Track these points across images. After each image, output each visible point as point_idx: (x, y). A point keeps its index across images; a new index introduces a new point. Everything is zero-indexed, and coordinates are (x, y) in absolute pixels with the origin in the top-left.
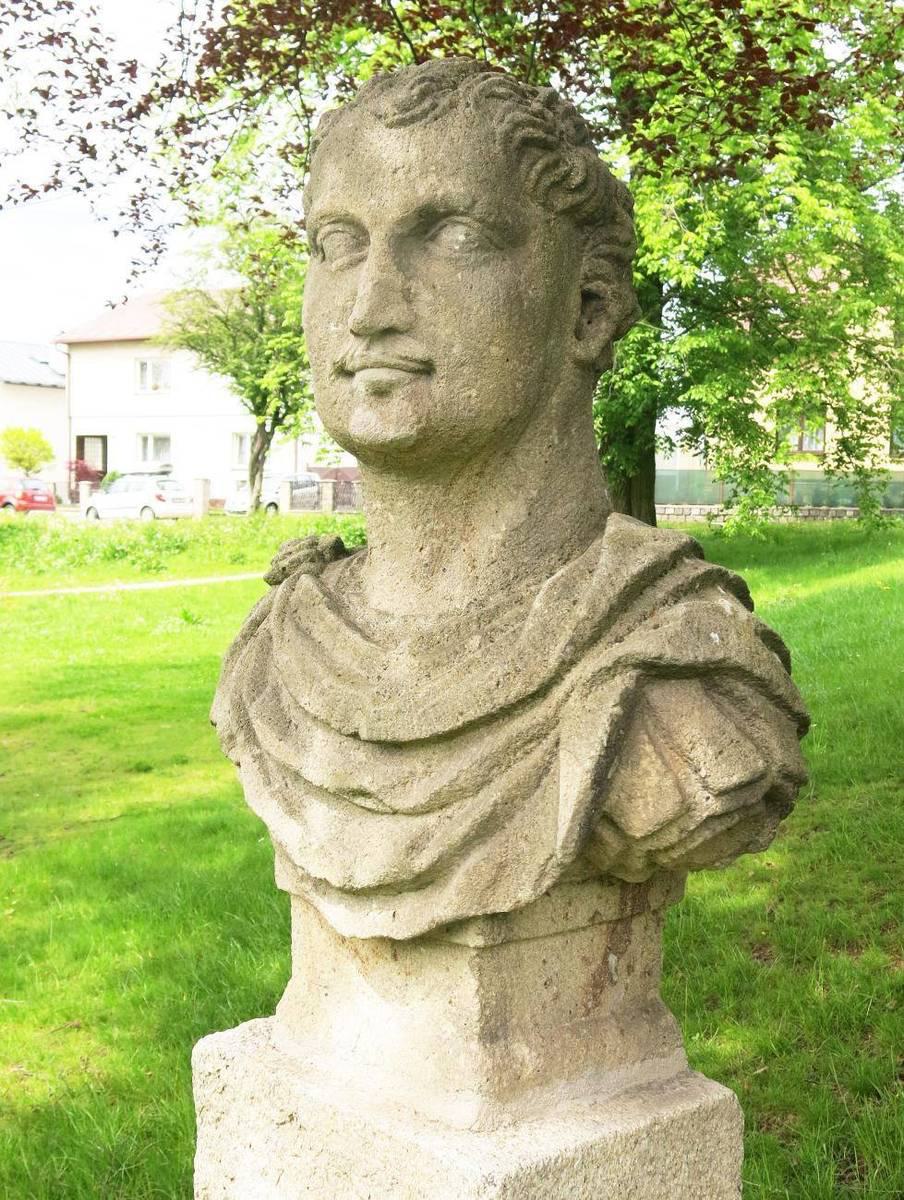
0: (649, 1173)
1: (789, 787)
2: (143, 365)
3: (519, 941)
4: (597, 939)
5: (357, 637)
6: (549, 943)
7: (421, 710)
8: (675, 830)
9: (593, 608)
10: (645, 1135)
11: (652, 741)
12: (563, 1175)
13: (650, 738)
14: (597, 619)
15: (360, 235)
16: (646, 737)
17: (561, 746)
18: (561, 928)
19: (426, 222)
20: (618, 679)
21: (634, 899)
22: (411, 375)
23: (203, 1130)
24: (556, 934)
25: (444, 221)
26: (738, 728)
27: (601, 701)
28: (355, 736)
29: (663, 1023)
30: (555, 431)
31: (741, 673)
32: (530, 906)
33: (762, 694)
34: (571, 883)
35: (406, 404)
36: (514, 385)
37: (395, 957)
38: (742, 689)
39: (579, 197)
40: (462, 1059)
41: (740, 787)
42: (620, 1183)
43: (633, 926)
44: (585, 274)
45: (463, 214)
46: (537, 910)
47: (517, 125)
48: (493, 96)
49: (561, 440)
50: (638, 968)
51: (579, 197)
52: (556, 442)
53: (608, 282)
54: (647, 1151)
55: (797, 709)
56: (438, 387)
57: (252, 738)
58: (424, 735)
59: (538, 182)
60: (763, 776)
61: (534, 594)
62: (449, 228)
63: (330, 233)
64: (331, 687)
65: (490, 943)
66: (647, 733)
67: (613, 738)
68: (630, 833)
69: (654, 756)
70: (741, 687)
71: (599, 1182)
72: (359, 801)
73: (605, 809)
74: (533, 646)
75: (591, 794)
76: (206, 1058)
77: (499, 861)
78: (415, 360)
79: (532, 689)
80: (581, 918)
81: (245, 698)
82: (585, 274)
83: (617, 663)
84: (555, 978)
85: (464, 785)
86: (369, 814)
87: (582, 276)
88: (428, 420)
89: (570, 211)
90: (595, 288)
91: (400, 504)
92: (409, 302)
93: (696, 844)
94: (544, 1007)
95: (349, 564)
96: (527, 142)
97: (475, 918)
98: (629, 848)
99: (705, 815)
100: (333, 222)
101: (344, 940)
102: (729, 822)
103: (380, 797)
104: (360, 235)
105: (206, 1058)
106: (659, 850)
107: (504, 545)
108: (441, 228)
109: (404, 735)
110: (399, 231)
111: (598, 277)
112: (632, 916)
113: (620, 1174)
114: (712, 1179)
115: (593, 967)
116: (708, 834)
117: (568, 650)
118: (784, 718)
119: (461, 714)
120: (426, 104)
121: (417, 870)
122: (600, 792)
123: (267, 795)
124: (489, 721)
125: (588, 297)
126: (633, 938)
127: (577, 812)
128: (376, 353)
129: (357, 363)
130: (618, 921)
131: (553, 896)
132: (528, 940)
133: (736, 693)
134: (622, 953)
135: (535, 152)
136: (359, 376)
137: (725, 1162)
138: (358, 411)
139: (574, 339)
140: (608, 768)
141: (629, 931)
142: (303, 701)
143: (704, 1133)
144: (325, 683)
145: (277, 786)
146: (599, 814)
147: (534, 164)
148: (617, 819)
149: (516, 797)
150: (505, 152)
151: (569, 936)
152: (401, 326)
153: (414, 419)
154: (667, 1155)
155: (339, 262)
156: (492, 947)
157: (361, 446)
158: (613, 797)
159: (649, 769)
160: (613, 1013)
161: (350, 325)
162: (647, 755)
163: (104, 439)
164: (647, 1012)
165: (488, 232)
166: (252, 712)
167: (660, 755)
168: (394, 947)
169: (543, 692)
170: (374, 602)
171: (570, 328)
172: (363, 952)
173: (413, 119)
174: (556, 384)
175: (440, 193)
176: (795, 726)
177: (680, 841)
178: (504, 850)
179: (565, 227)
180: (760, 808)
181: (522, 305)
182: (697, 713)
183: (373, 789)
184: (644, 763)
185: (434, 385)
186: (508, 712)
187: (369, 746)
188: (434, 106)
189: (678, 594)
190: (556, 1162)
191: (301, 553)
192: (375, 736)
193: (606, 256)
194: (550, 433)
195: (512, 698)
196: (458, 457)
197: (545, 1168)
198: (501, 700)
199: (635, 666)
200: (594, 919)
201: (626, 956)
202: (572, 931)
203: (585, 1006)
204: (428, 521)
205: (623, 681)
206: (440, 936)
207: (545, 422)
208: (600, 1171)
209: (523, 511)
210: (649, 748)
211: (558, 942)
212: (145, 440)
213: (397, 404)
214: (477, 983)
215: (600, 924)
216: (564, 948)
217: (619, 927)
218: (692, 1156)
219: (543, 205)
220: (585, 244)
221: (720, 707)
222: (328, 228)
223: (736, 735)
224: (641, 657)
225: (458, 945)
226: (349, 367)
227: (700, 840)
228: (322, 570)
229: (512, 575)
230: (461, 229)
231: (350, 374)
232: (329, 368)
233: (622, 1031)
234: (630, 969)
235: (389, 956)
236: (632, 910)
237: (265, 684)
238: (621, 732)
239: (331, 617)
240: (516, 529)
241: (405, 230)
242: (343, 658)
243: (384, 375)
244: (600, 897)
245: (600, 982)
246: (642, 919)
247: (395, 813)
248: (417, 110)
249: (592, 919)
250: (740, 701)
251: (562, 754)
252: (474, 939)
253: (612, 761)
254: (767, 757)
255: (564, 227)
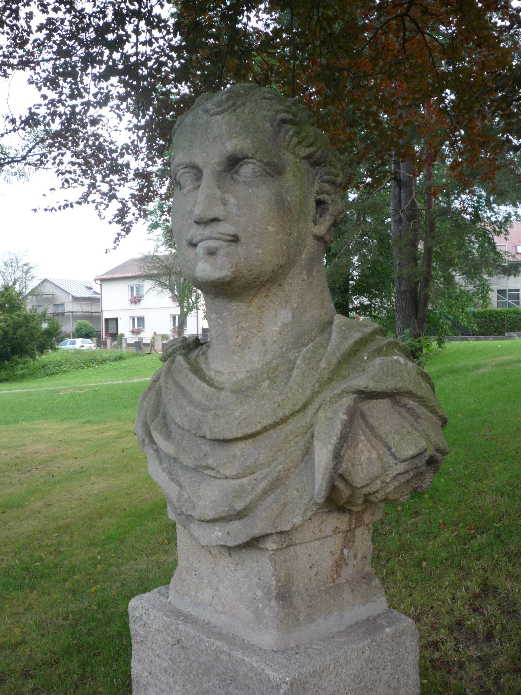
0: (370, 669)
1: (438, 455)
2: (132, 288)
3: (295, 545)
4: (338, 540)
5: (204, 385)
6: (312, 544)
7: (237, 422)
8: (379, 482)
9: (329, 363)
10: (367, 648)
11: (364, 434)
12: (324, 675)
13: (363, 432)
14: (331, 368)
15: (197, 172)
16: (361, 432)
17: (315, 438)
18: (318, 536)
19: (234, 163)
20: (344, 400)
21: (356, 519)
22: (227, 243)
23: (135, 647)
24: (315, 540)
25: (241, 163)
26: (412, 425)
27: (335, 413)
28: (204, 437)
29: (373, 584)
30: (305, 272)
31: (410, 394)
32: (301, 525)
33: (422, 405)
34: (322, 512)
35: (224, 258)
36: (282, 247)
37: (230, 554)
38: (411, 403)
39: (312, 150)
40: (266, 612)
41: (414, 457)
42: (355, 676)
43: (356, 533)
44: (317, 191)
45: (251, 158)
46: (305, 528)
47: (278, 112)
48: (265, 99)
49: (308, 278)
50: (359, 555)
51: (312, 150)
52: (306, 278)
53: (329, 194)
54: (369, 657)
55: (440, 414)
56: (241, 249)
57: (152, 441)
58: (240, 435)
59: (290, 142)
60: (425, 451)
61: (296, 358)
62: (244, 166)
63: (183, 173)
64: (190, 411)
65: (280, 547)
66: (361, 429)
67: (343, 433)
68: (354, 485)
69: (366, 442)
70: (411, 402)
71: (343, 676)
72: (207, 472)
73: (339, 472)
74: (298, 384)
75: (332, 464)
76: (135, 609)
77: (283, 502)
78: (229, 235)
79: (298, 407)
80: (328, 529)
81: (148, 420)
82: (317, 191)
83: (343, 391)
84: (316, 564)
85: (262, 462)
86: (213, 479)
87: (315, 191)
88: (237, 266)
89: (308, 158)
90: (322, 198)
91: (225, 314)
92: (225, 205)
93: (390, 489)
94: (310, 580)
95: (201, 349)
96: (284, 121)
97: (271, 534)
98: (354, 492)
99: (395, 474)
100: (184, 168)
101: (203, 546)
102: (407, 477)
103: (218, 470)
104: (197, 172)
105: (135, 609)
106: (370, 494)
107: (280, 333)
108: (240, 166)
109: (229, 436)
110: (218, 169)
111: (324, 192)
112: (356, 528)
113: (355, 671)
114: (403, 668)
115: (336, 556)
116: (396, 483)
117: (316, 386)
118: (435, 418)
119: (260, 423)
120: (230, 103)
121: (238, 508)
122: (337, 463)
123: (160, 470)
124: (274, 425)
125: (319, 203)
126: (356, 539)
127: (324, 475)
128: (207, 231)
129: (199, 238)
130: (348, 531)
131: (313, 519)
132: (300, 544)
133: (409, 406)
134: (351, 548)
135: (288, 126)
136: (200, 245)
137: (410, 659)
138: (200, 264)
139: (313, 224)
140: (341, 449)
141: (354, 536)
142: (178, 420)
143: (398, 644)
144: (188, 409)
145: (165, 465)
146: (338, 478)
147: (288, 132)
148: (347, 477)
149: (291, 467)
150: (272, 126)
151: (322, 540)
152: (221, 218)
153: (229, 266)
154: (380, 658)
155: (188, 188)
156: (281, 549)
157: (202, 283)
158: (344, 465)
159: (363, 449)
160: (347, 581)
161: (194, 219)
162: (362, 441)
163: (116, 319)
164: (365, 578)
165: (265, 167)
166: (152, 426)
167: (369, 441)
168: (231, 550)
169: (305, 407)
170: (213, 366)
171: (311, 219)
172: (214, 552)
173: (223, 111)
174: (304, 248)
175: (238, 148)
176: (440, 423)
177: (382, 488)
178: (285, 496)
179: (306, 166)
180: (424, 468)
181: (284, 204)
182: (389, 418)
183: (215, 465)
184: (360, 446)
185: (239, 248)
186: (284, 420)
187: (211, 442)
188: (234, 104)
189: (379, 352)
190: (320, 667)
191: (178, 345)
192: (213, 437)
193: (327, 182)
194: (302, 274)
195: (287, 412)
196: (255, 287)
197: (314, 671)
198: (280, 414)
199: (354, 393)
200: (336, 530)
201: (353, 550)
202: (323, 538)
203: (332, 577)
204: (240, 322)
205: (347, 401)
206: (253, 543)
207: (299, 268)
208: (344, 670)
209: (290, 315)
210: (363, 438)
211: (317, 543)
212: (133, 319)
213: (221, 258)
214: (274, 569)
215: (339, 533)
216: (320, 547)
217: (349, 534)
218: (393, 657)
219: (294, 154)
220: (316, 175)
221: (400, 413)
222: (182, 171)
223: (410, 429)
224: (357, 387)
225: (262, 549)
226: (194, 241)
227: (393, 487)
228: (188, 354)
229: (285, 348)
230: (250, 166)
231: (195, 245)
232: (184, 243)
233: (352, 591)
234: (355, 556)
235: (227, 554)
236: (356, 525)
237: (159, 412)
238: (348, 429)
239: (191, 376)
240: (287, 324)
241: (222, 169)
242: (197, 396)
243: (212, 244)
244: (338, 519)
245: (340, 564)
246: (361, 529)
247: (226, 478)
248: (226, 106)
249: (334, 531)
250: (410, 410)
251: (315, 444)
252: (271, 545)
253: (343, 446)
254: (428, 438)
255: (305, 165)
